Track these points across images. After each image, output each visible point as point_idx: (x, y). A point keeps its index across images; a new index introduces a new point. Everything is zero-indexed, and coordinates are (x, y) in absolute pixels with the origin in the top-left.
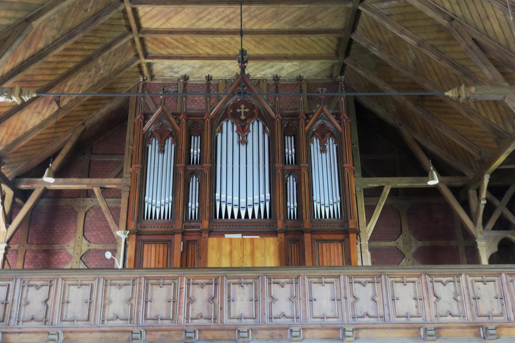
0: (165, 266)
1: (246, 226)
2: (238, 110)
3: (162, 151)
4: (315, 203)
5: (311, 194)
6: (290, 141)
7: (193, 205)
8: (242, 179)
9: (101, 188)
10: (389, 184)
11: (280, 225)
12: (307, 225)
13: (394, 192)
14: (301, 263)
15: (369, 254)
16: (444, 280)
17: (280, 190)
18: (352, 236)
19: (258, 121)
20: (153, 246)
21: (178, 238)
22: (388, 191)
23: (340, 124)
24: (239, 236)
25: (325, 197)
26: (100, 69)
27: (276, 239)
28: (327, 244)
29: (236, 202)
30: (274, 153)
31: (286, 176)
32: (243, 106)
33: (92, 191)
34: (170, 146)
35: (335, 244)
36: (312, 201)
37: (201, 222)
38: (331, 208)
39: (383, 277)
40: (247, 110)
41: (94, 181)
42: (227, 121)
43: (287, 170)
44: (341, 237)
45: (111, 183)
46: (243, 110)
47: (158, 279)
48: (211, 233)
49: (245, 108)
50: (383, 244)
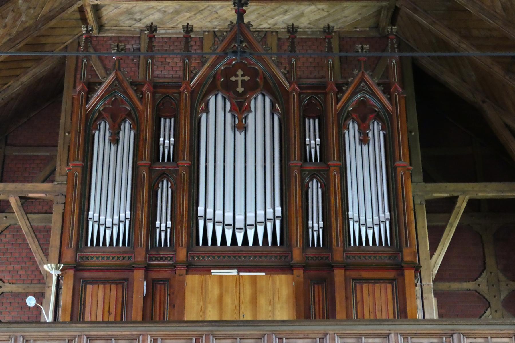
0: (119, 319)
1: (243, 256)
2: (233, 79)
3: (115, 140)
4: (351, 222)
5: (345, 208)
6: (312, 126)
7: (163, 224)
8: (239, 190)
9: (21, 197)
10: (466, 192)
11: (297, 255)
12: (338, 256)
13: (474, 205)
14: (329, 314)
15: (434, 301)
17: (296, 201)
18: (409, 274)
19: (264, 96)
20: (101, 287)
21: (139, 275)
22: (465, 204)
23: (390, 100)
24: (233, 272)
25: (367, 213)
26: (21, 15)
27: (289, 277)
28: (370, 285)
29: (229, 220)
30: (289, 146)
31: (307, 180)
32: (240, 72)
33: (8, 202)
34: (127, 133)
35: (383, 285)
36: (346, 220)
37: (175, 251)
38: (376, 229)
39: (455, 336)
40: (247, 78)
41: (11, 186)
43: (308, 172)
44: (391, 274)
45: (37, 190)
46: (240, 79)
48: (190, 267)
49: (243, 76)
50: (455, 286)
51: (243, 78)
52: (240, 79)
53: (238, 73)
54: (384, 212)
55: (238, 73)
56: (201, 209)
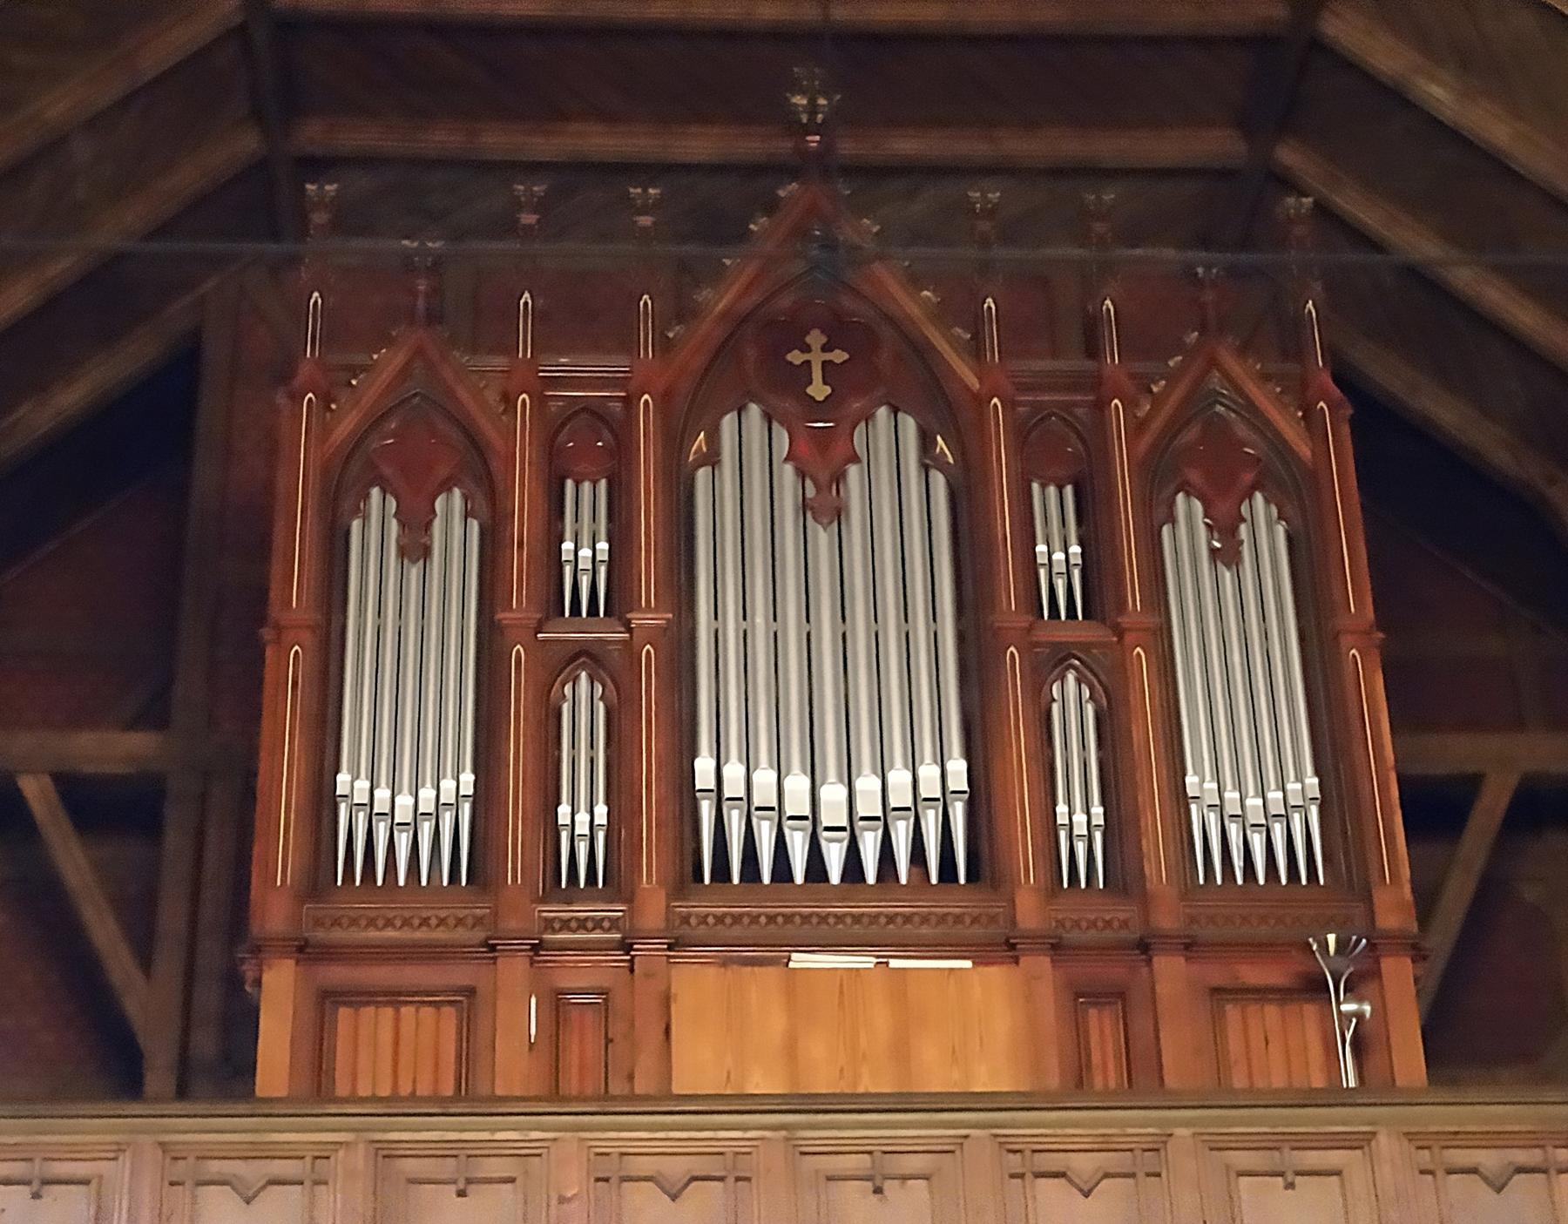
2: (796, 357)
3: (415, 548)
16: (1083, 1164)
29: (797, 803)
38: (1278, 831)
40: (839, 356)
42: (741, 410)
46: (817, 359)
47: (444, 1152)
51: (828, 356)
52: (817, 359)
53: (808, 339)
54: (1299, 778)
55: (808, 339)
56: (704, 767)
